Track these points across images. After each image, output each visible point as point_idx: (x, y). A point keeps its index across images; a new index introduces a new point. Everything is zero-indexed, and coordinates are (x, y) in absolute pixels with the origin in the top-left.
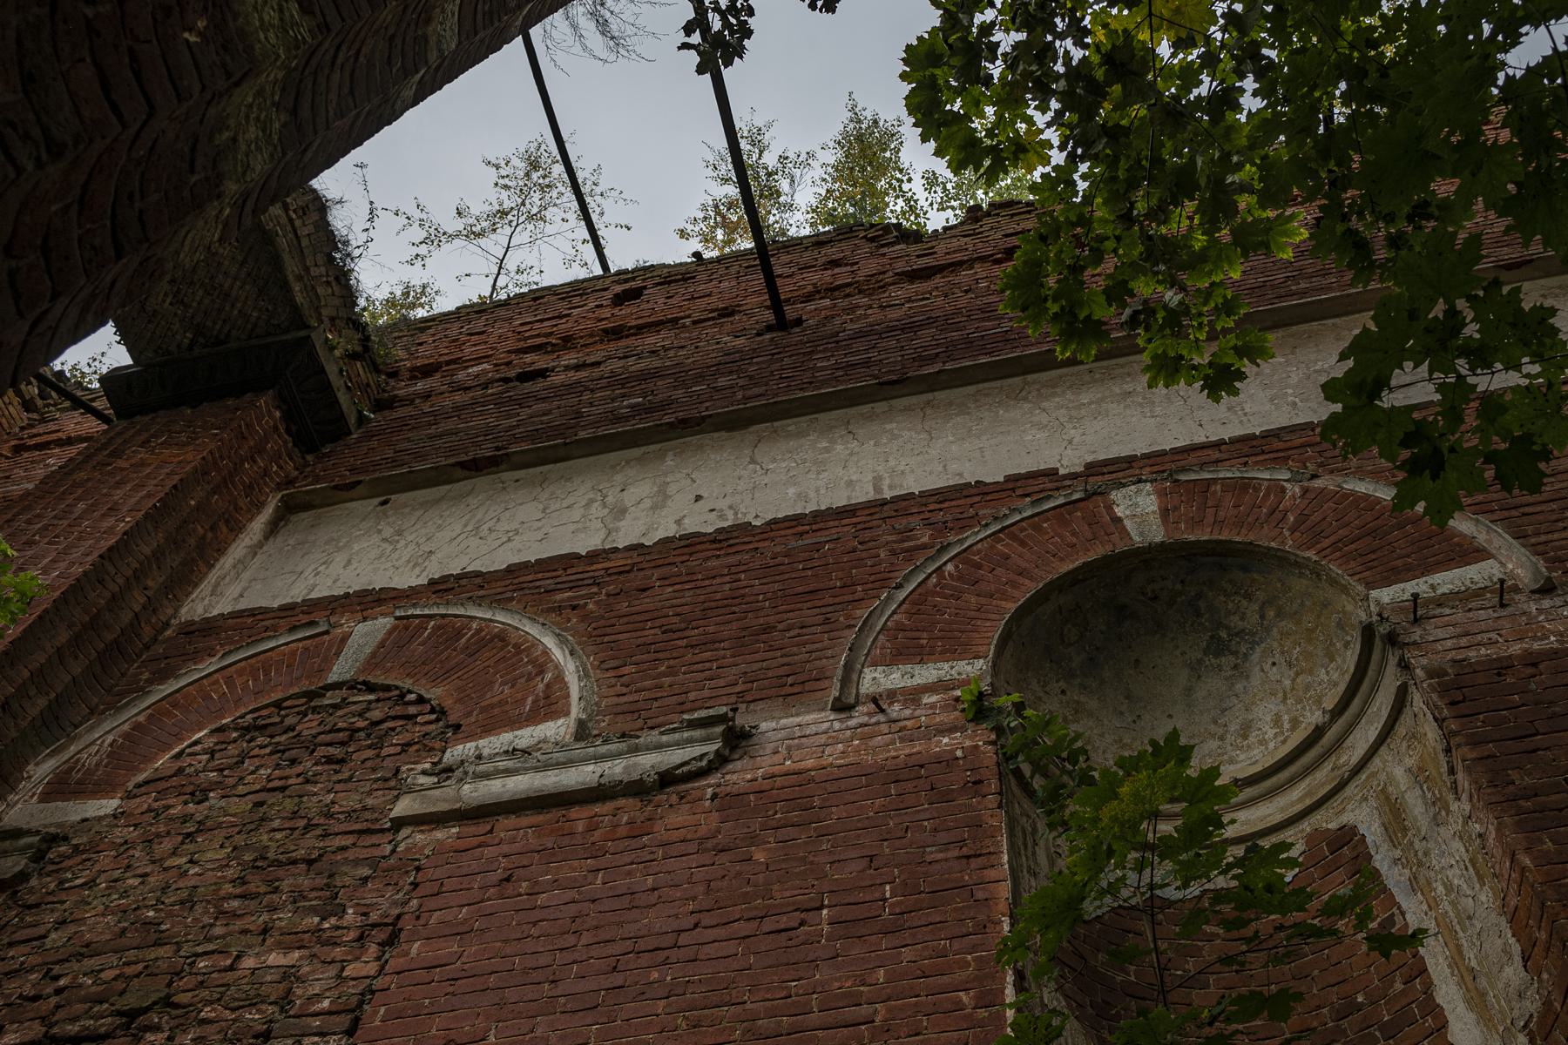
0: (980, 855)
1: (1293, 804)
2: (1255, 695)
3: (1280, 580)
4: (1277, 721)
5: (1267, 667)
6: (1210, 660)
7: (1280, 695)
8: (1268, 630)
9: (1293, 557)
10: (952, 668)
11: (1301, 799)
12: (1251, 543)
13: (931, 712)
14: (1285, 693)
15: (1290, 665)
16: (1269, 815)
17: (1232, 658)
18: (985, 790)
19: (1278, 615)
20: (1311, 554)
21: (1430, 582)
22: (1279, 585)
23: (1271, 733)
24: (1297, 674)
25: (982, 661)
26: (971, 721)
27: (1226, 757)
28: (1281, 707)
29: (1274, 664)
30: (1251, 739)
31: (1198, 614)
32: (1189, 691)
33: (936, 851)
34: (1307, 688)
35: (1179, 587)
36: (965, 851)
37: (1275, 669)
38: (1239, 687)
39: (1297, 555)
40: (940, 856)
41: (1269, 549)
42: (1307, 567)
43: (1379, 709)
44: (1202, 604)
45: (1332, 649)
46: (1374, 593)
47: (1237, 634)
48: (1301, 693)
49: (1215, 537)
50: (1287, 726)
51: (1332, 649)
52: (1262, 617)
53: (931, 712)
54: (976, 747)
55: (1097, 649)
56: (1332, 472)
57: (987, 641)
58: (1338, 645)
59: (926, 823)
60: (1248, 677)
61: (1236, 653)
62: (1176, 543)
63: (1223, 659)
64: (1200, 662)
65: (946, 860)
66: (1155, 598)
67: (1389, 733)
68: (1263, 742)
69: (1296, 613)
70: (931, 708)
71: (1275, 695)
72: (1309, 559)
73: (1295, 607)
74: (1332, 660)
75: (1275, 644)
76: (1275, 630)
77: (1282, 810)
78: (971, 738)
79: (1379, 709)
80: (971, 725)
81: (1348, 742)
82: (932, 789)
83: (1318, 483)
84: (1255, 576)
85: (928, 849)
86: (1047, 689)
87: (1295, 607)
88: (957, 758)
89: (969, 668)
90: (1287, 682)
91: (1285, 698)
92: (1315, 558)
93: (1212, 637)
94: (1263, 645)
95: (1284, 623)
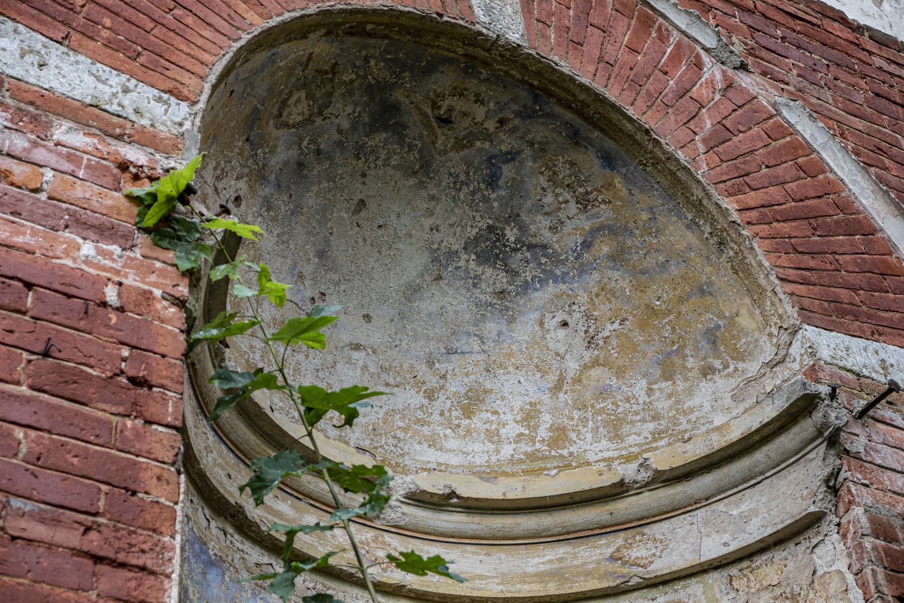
0: (123, 565)
1: (524, 578)
2: (511, 355)
3: (651, 210)
4: (530, 416)
5: (551, 323)
6: (468, 262)
7: (552, 378)
8: (583, 270)
9: (700, 194)
10: (126, 91)
11: (541, 577)
12: (647, 132)
13: (66, 166)
14: (561, 380)
15: (591, 342)
16: (481, 577)
17: (503, 278)
18: (153, 410)
19: (612, 257)
20: (729, 204)
21: (882, 355)
22: (645, 216)
23: (512, 429)
24: (596, 363)
25: (184, 107)
26: (147, 231)
27: (426, 430)
28: (546, 398)
29: (399, 215)
30: (477, 422)
31: (492, 181)
32: (413, 291)
33: (31, 516)
34: (603, 393)
35: (491, 125)
36: (94, 542)
37: (562, 333)
38: (492, 327)
39: (708, 196)
40: (38, 530)
41: (670, 157)
42: (713, 221)
43: (745, 518)
44: (507, 171)
45: (677, 361)
46: (810, 332)
47: (531, 247)
48: (588, 395)
49: (598, 86)
50: (543, 432)
51: (677, 361)
52: (587, 245)
53: (66, 166)
54: (147, 296)
55: (318, 152)
56: (764, 74)
57: (198, 69)
58: (691, 362)
59: (19, 433)
60: (512, 320)
61: (513, 273)
62: (537, 60)
63: (489, 271)
64: (452, 255)
65: (50, 546)
66: (445, 121)
67: (740, 560)
68: (493, 436)
69: (644, 272)
70: (69, 158)
71: (542, 370)
72: (725, 212)
73: (649, 262)
74: (668, 375)
75: (583, 297)
76: (596, 276)
77: (504, 579)
78: (144, 270)
79: (745, 518)
80: (141, 239)
81: (657, 530)
82: (46, 354)
83: (745, 81)
84: (618, 181)
85: (16, 503)
86: (220, 185)
87: (649, 262)
88: (104, 304)
89: (159, 109)
90: (572, 366)
91: (558, 387)
92: (735, 216)
93: (491, 229)
94: (563, 287)
95: (616, 275)
